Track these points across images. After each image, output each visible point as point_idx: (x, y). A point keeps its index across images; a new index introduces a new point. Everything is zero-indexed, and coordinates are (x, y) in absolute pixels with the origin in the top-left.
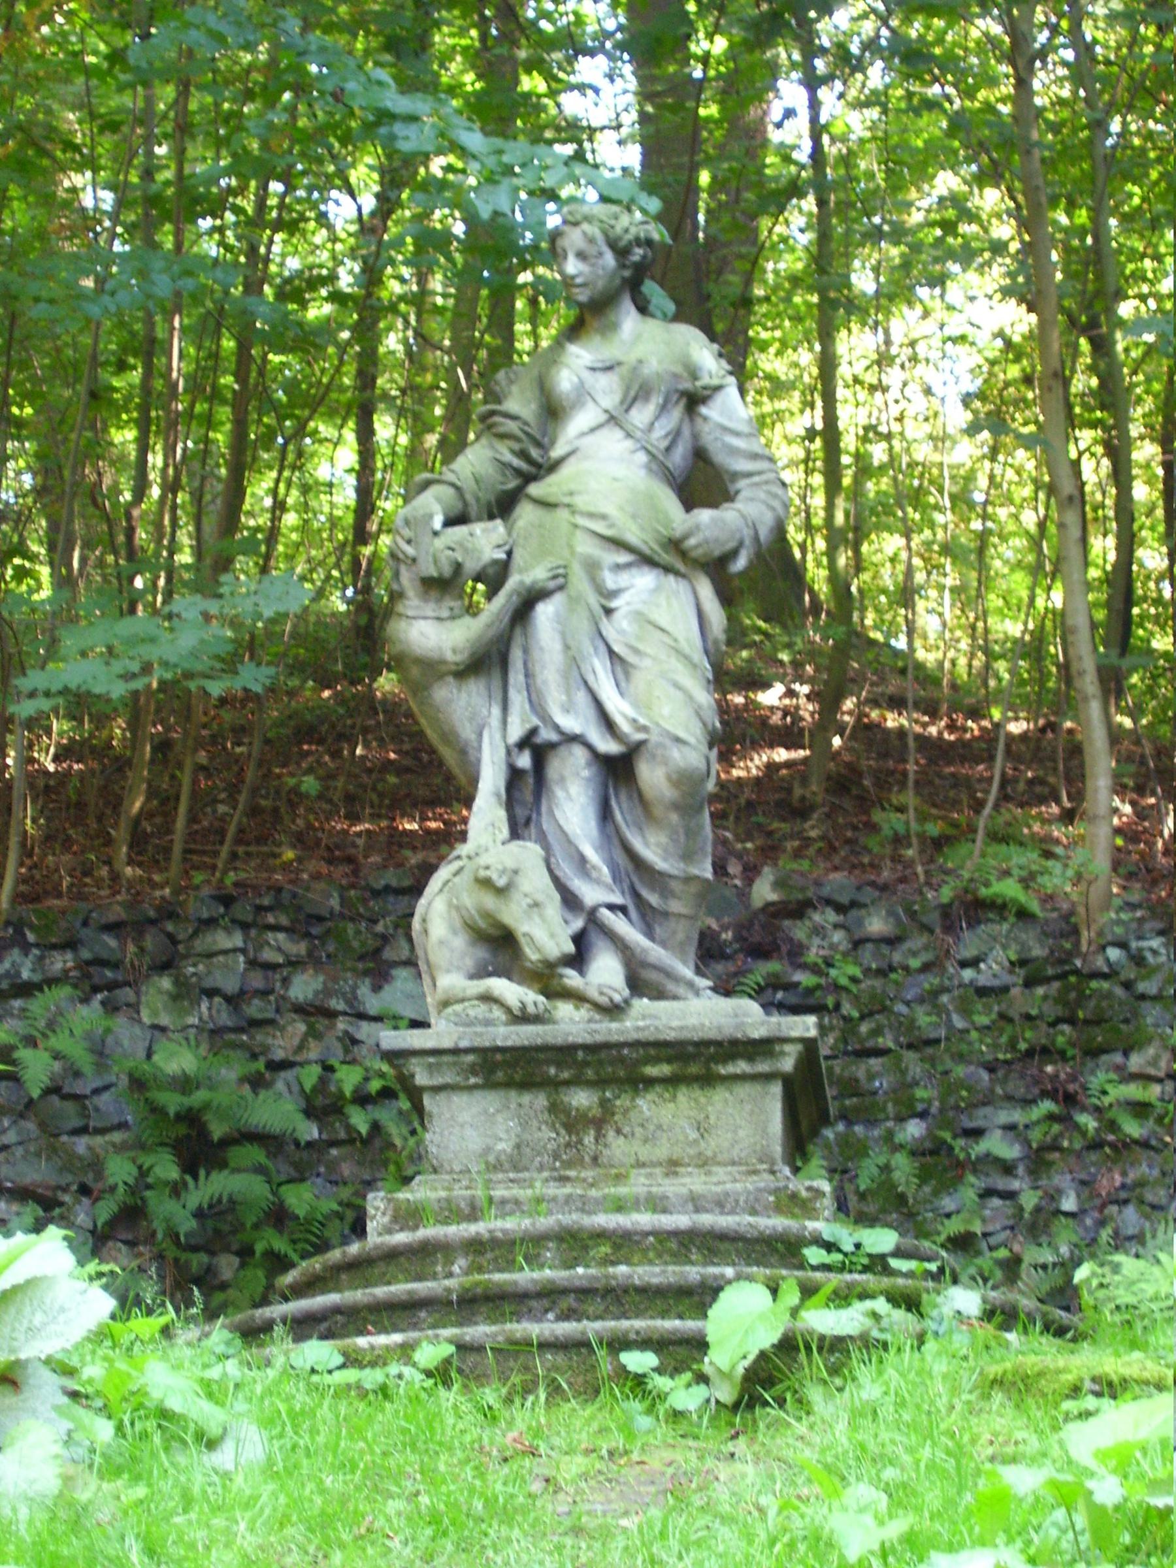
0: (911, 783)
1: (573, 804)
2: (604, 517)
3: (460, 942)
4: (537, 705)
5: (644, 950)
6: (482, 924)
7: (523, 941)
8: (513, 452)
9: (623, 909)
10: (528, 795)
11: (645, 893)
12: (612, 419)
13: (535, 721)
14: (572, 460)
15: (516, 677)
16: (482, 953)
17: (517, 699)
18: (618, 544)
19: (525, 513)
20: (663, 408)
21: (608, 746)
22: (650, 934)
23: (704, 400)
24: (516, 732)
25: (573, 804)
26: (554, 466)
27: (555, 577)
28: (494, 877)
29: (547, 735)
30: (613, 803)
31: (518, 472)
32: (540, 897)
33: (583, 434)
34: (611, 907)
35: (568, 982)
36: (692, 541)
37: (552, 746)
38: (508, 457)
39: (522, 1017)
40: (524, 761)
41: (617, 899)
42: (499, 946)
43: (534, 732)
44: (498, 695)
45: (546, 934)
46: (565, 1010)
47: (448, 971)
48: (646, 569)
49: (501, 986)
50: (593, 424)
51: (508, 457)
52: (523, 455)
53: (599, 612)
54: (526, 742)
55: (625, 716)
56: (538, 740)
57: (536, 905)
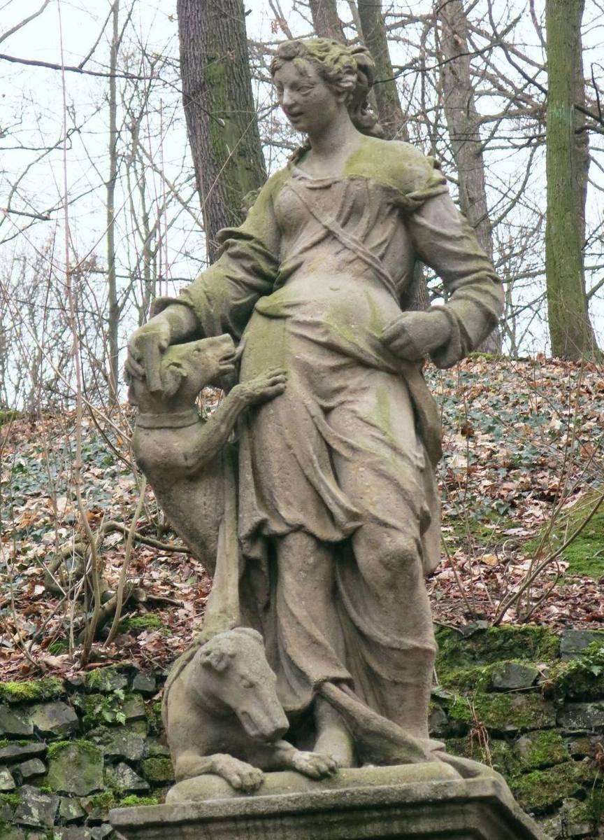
0: (76, 597)
1: (299, 591)
2: (316, 325)
3: (192, 718)
4: (264, 498)
5: (367, 720)
6: (209, 703)
7: (243, 719)
8: (247, 271)
9: (349, 682)
10: (260, 582)
11: (376, 667)
12: (329, 235)
13: (263, 515)
14: (298, 274)
15: (247, 476)
16: (211, 732)
17: (249, 496)
18: (331, 348)
19: (256, 325)
20: (377, 219)
21: (337, 536)
22: (384, 709)
23: (418, 210)
24: (247, 526)
25: (299, 591)
26: (283, 280)
27: (274, 383)
28: (214, 663)
29: (276, 527)
30: (341, 587)
31: (251, 288)
32: (254, 678)
33: (306, 249)
34: (337, 681)
35: (287, 755)
36: (398, 342)
37: (282, 537)
38: (241, 275)
39: (242, 790)
40: (257, 552)
41: (344, 674)
42: (224, 726)
43: (262, 524)
44: (230, 494)
45: (268, 712)
46: (273, 779)
47: (185, 748)
48: (359, 370)
49: (223, 760)
50: (315, 238)
51: (241, 275)
52: (256, 272)
53: (317, 412)
54: (258, 533)
55: (341, 507)
56: (265, 532)
57: (252, 685)
